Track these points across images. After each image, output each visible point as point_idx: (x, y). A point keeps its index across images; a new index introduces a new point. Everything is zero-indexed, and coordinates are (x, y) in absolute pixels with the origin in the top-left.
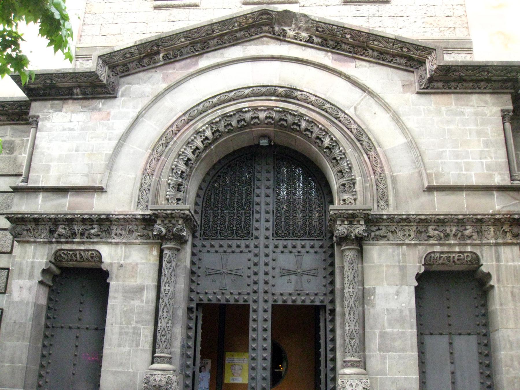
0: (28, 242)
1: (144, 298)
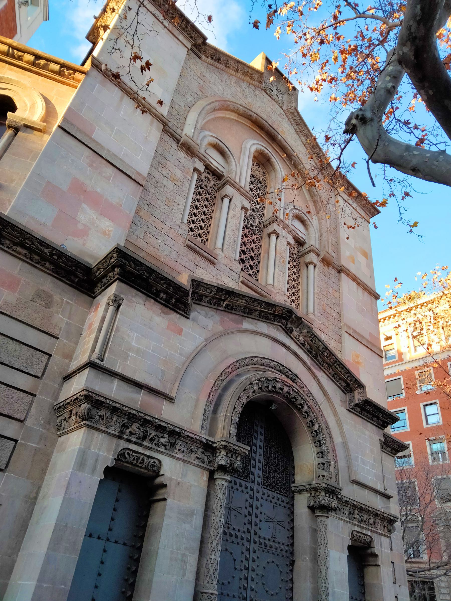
0: (97, 429)
1: (193, 523)
